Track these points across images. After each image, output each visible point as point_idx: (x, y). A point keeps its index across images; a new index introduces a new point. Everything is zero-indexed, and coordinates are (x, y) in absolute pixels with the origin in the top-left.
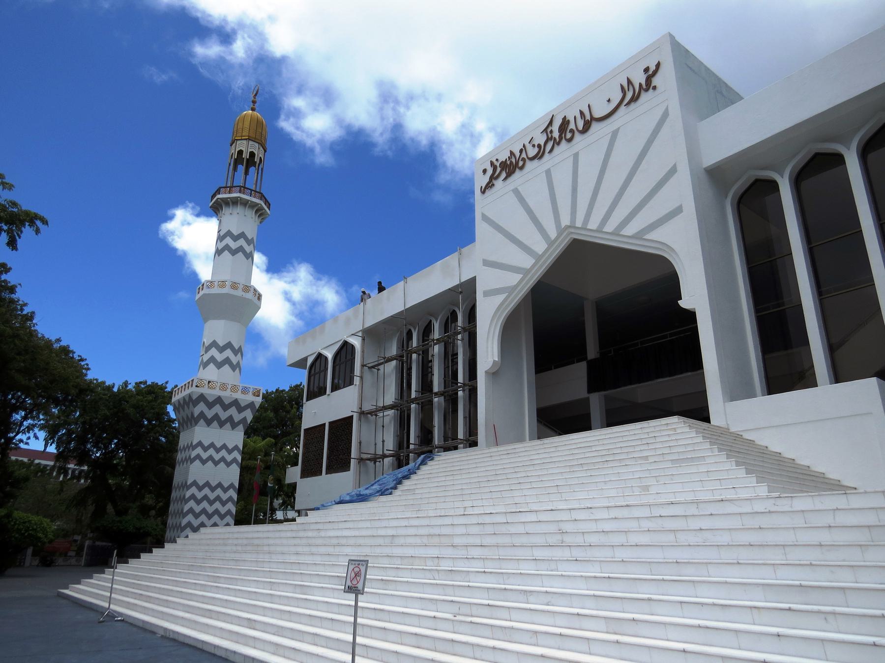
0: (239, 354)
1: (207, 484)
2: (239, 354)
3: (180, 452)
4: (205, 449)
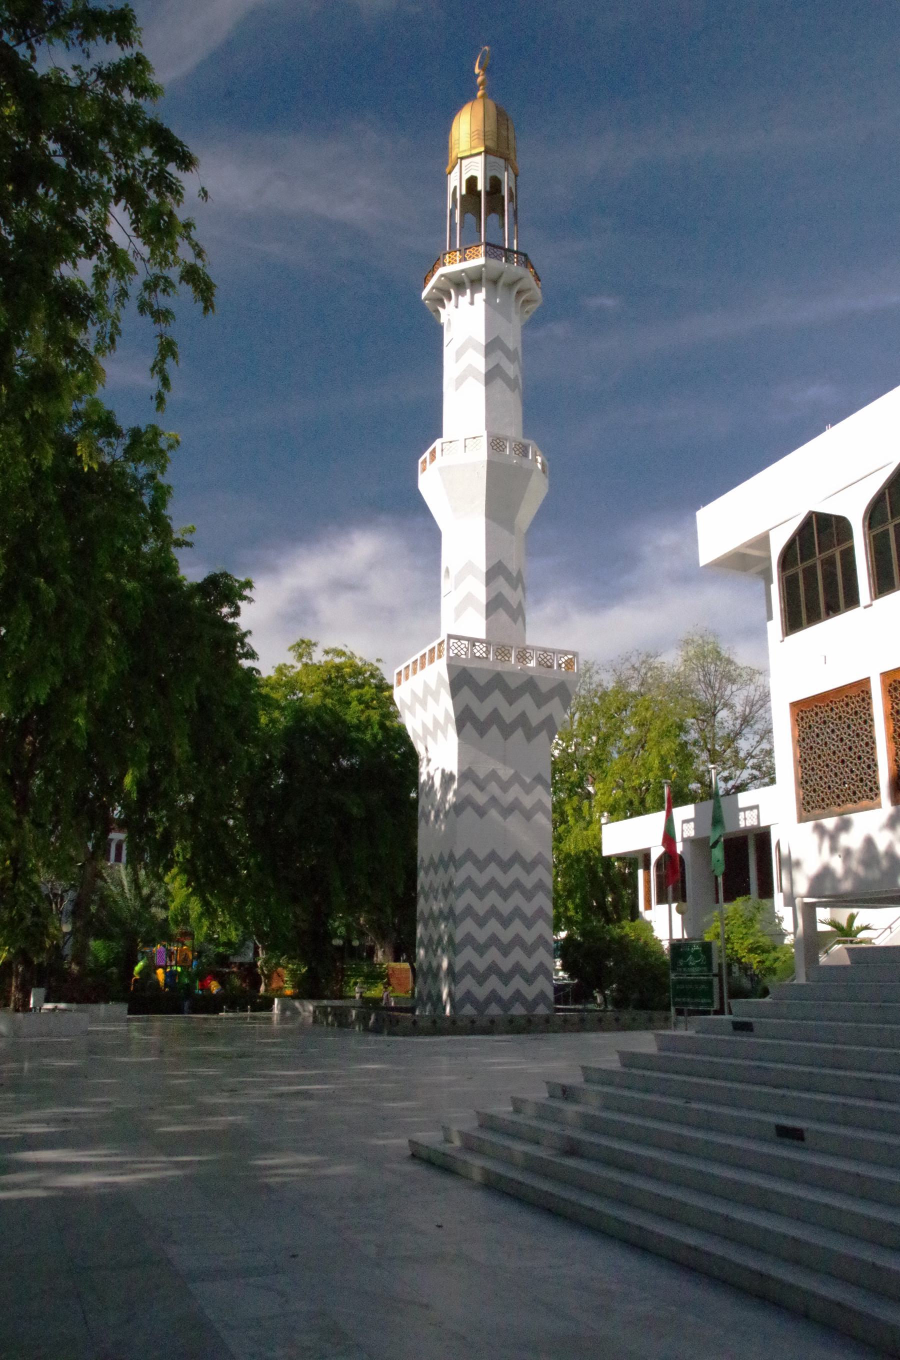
0: (520, 588)
1: (493, 857)
2: (520, 588)
3: (422, 896)
4: (481, 866)
